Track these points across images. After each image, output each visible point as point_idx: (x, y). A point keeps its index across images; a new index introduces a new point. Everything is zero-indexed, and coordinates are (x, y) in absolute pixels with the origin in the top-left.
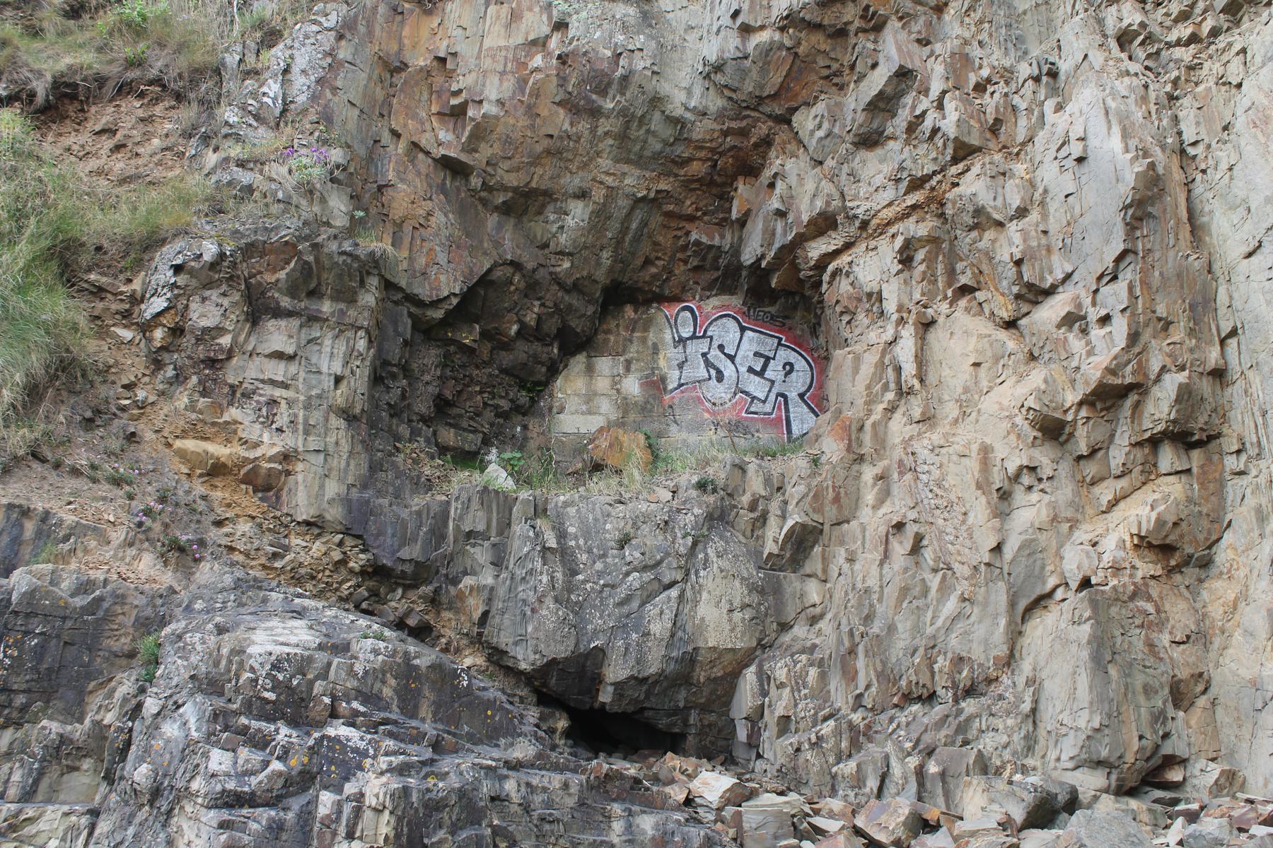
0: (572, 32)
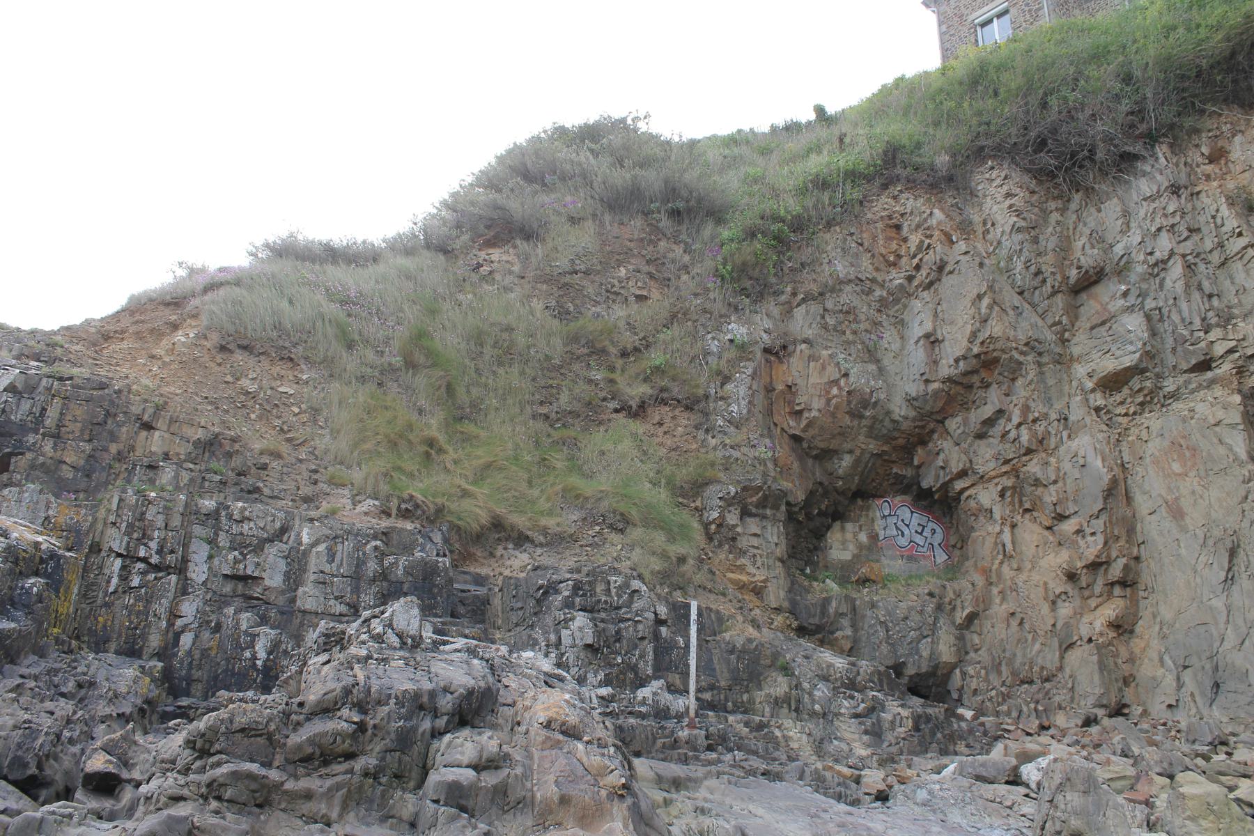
0: (852, 379)
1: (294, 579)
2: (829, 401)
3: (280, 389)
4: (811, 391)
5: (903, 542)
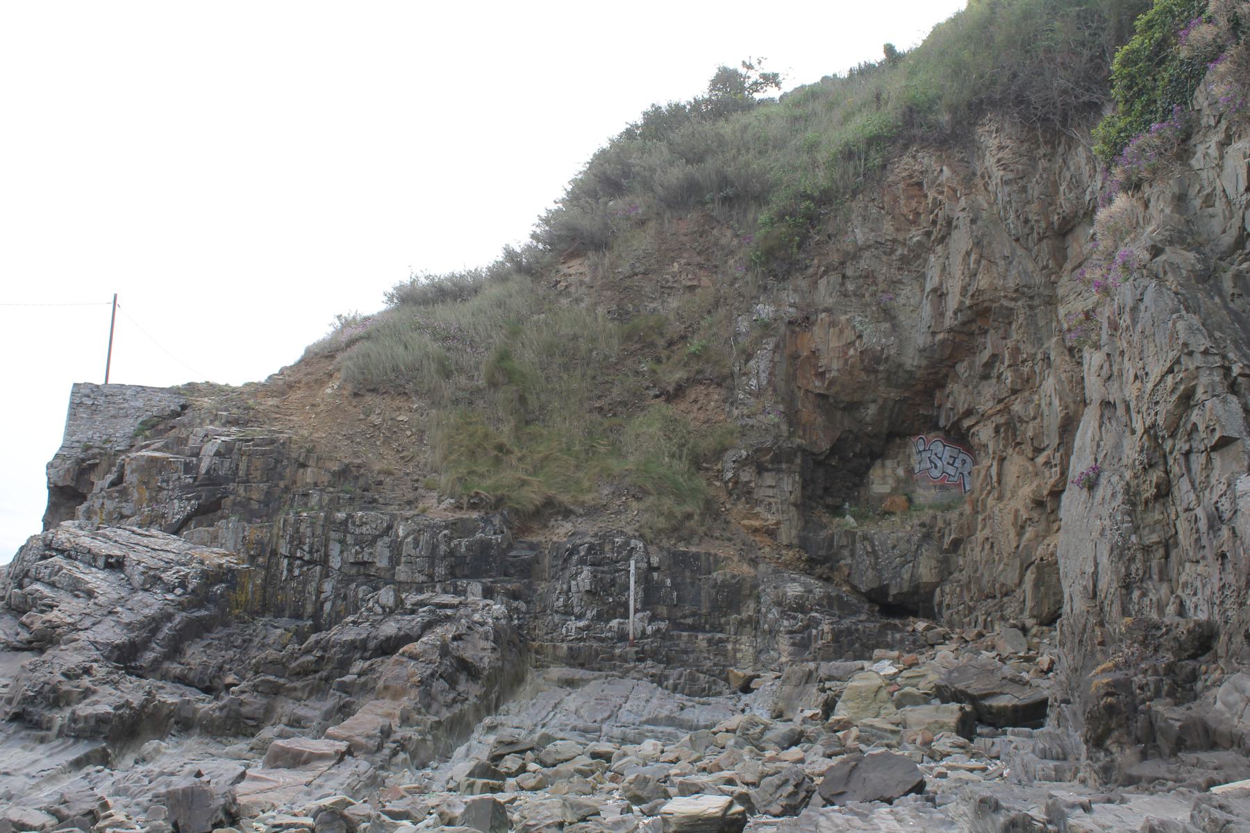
0: (864, 340)
1: (394, 561)
2: (846, 361)
3: (399, 418)
4: (832, 354)
5: (936, 473)
